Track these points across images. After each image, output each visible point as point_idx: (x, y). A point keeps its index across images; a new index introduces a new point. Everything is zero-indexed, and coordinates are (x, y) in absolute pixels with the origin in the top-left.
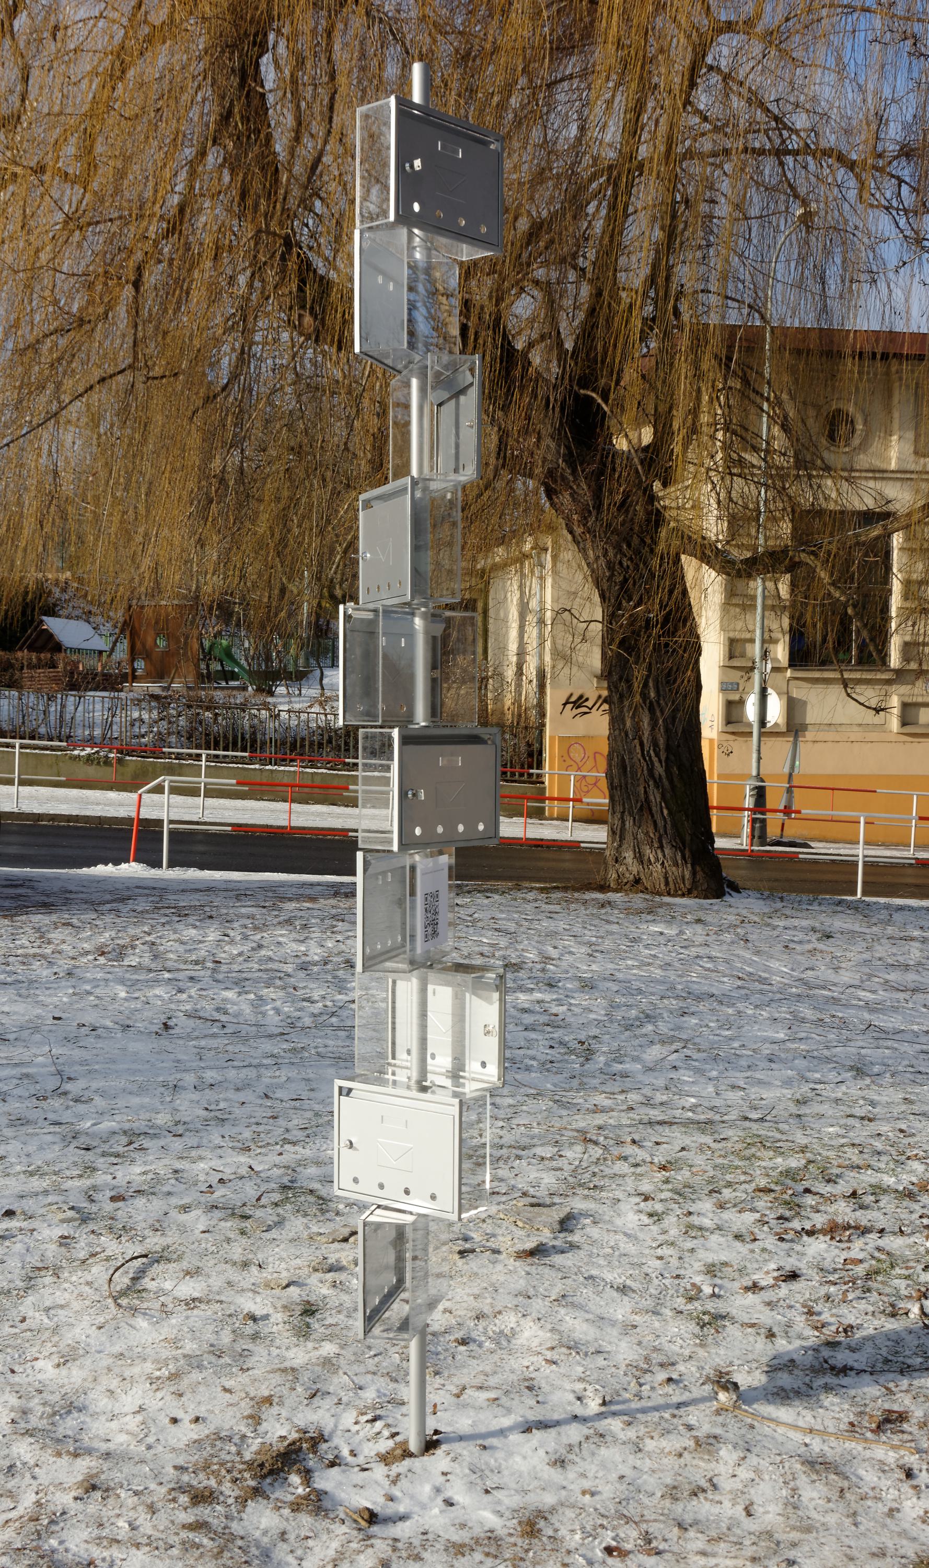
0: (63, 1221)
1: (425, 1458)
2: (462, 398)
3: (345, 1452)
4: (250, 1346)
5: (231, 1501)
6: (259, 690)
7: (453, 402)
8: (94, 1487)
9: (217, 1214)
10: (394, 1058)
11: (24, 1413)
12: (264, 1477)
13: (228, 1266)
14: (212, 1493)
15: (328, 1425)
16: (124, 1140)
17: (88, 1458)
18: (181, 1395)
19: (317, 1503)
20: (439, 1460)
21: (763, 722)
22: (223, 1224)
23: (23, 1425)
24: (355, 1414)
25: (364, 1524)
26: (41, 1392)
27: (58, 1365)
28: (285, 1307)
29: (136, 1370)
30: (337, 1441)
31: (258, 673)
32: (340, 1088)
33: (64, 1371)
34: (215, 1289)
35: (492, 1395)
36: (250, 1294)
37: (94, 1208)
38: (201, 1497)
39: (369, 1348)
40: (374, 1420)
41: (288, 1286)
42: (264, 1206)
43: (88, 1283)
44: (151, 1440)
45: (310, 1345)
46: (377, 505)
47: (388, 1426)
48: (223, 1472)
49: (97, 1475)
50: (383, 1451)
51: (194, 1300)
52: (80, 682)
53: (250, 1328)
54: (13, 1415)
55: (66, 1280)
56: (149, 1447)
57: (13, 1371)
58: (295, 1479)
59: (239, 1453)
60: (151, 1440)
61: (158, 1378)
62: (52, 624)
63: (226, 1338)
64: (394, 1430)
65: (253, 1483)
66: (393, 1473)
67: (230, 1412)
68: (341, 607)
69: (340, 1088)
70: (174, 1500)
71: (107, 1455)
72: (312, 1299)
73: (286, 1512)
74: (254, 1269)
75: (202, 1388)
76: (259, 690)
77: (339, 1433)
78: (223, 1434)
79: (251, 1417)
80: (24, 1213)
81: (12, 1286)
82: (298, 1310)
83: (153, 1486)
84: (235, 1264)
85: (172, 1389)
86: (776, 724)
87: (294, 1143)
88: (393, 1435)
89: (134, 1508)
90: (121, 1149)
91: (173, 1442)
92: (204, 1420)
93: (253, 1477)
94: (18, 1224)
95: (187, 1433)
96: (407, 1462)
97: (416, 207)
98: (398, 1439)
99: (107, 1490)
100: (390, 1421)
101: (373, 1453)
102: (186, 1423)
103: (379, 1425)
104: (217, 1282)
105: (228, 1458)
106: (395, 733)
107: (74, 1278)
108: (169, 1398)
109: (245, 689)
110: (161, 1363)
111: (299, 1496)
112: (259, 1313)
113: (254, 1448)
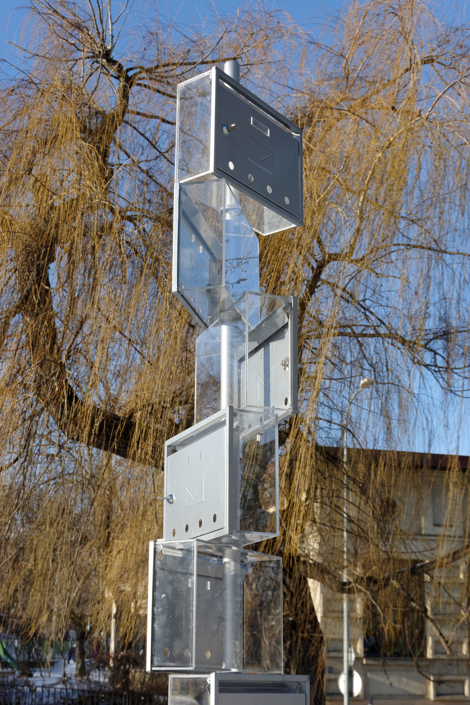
2: (273, 345)
6: (23, 674)
7: (262, 350)
21: (350, 693)
31: (23, 662)
46: (181, 452)
68: (151, 544)
76: (23, 674)
86: (358, 696)
97: (231, 166)
106: (211, 679)
109: (13, 673)
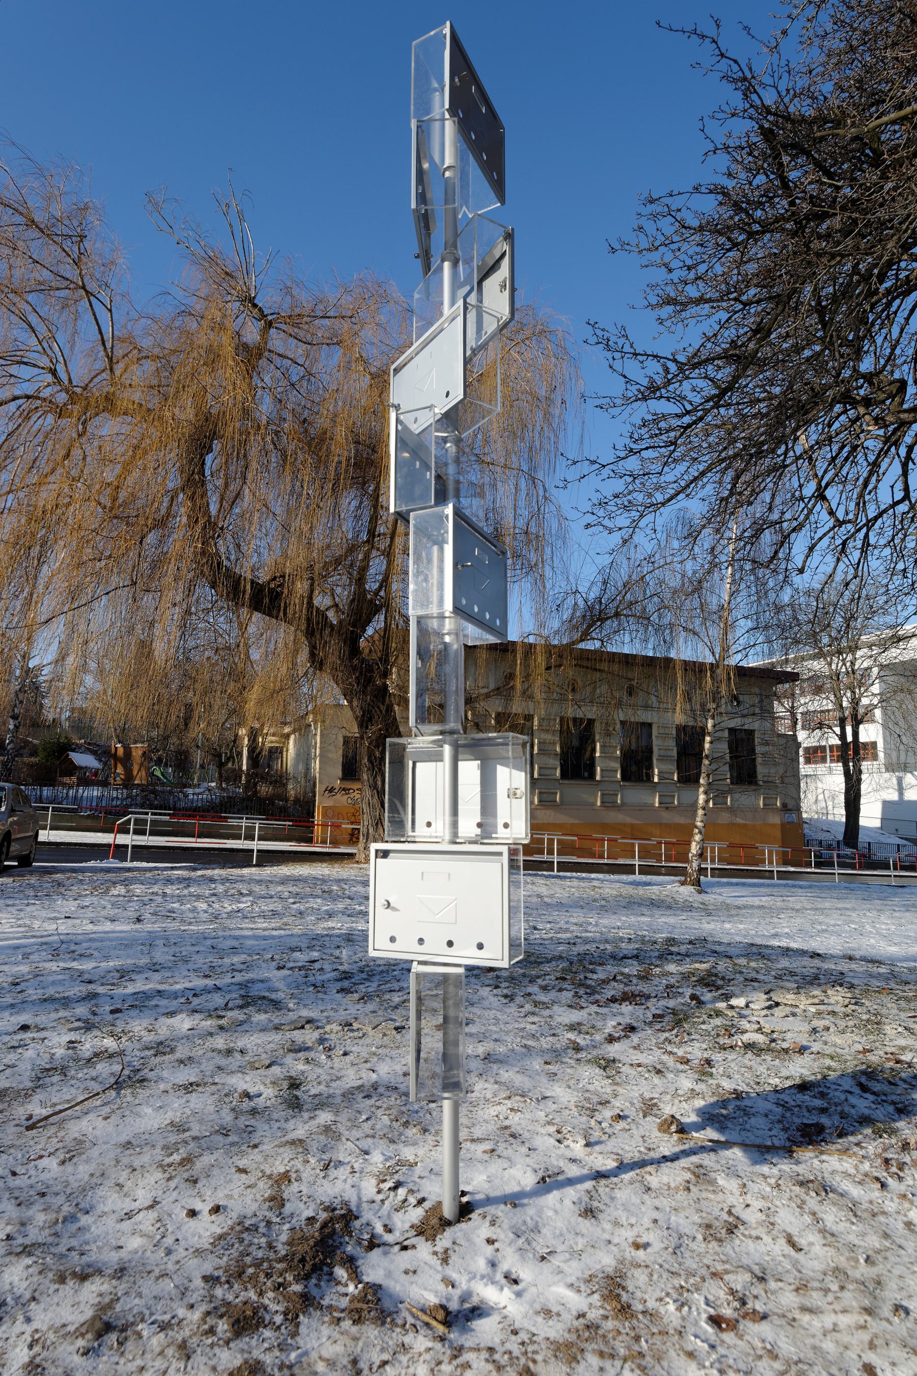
0: (71, 1030)
1: (463, 1226)
3: (379, 1229)
4: (252, 1122)
5: (278, 1319)
8: (108, 1327)
9: (198, 1016)
10: (413, 831)
11: (23, 1224)
12: (307, 1277)
13: (215, 1054)
14: (255, 1311)
15: (351, 1196)
16: (117, 975)
17: (97, 1280)
18: (196, 1182)
19: (376, 1306)
20: (477, 1228)
22: (203, 1023)
23: (20, 1240)
24: (374, 1182)
25: (441, 1329)
26: (43, 1195)
27: (63, 1162)
28: (273, 1083)
29: (146, 1158)
30: (367, 1215)
32: (377, 851)
33: (69, 1168)
34: (208, 1073)
35: (488, 1146)
36: (240, 1075)
37: (97, 1019)
38: (246, 1322)
39: (359, 1112)
40: (395, 1188)
41: (269, 1066)
42: (231, 1009)
43: (93, 1079)
44: (169, 1241)
45: (306, 1115)
47: (411, 1191)
48: (262, 1278)
49: (110, 1306)
50: (416, 1221)
51: (191, 1084)
52: (85, 782)
53: (246, 1105)
54: (9, 1229)
55: (72, 1078)
56: (169, 1252)
57: (14, 1174)
58: (341, 1273)
59: (270, 1246)
60: (169, 1241)
61: (170, 1165)
62: (73, 756)
63: (227, 1117)
64: (419, 1196)
65: (297, 1288)
66: (439, 1249)
67: (249, 1195)
69: (377, 851)
70: (212, 1331)
71: (121, 1272)
72: (293, 1074)
73: (347, 1324)
74: (237, 1055)
75: (216, 1171)
77: (365, 1205)
78: (248, 1223)
79: (272, 1199)
80: (36, 1026)
81: (21, 1086)
82: (285, 1085)
83: (181, 1312)
84: (220, 1052)
85: (186, 1175)
87: (241, 971)
88: (421, 1201)
89: (161, 1353)
90: (115, 981)
91: (195, 1242)
92: (225, 1208)
93: (297, 1279)
94: (31, 1035)
95: (206, 1228)
96: (449, 1232)
98: (427, 1205)
99: (123, 1330)
100: (411, 1186)
101: (407, 1226)
102: (205, 1216)
103: (402, 1192)
104: (208, 1067)
105: (260, 1254)
107: (80, 1075)
108: (183, 1186)
110: (169, 1149)
111: (354, 1299)
112: (252, 1091)
113: (284, 1237)
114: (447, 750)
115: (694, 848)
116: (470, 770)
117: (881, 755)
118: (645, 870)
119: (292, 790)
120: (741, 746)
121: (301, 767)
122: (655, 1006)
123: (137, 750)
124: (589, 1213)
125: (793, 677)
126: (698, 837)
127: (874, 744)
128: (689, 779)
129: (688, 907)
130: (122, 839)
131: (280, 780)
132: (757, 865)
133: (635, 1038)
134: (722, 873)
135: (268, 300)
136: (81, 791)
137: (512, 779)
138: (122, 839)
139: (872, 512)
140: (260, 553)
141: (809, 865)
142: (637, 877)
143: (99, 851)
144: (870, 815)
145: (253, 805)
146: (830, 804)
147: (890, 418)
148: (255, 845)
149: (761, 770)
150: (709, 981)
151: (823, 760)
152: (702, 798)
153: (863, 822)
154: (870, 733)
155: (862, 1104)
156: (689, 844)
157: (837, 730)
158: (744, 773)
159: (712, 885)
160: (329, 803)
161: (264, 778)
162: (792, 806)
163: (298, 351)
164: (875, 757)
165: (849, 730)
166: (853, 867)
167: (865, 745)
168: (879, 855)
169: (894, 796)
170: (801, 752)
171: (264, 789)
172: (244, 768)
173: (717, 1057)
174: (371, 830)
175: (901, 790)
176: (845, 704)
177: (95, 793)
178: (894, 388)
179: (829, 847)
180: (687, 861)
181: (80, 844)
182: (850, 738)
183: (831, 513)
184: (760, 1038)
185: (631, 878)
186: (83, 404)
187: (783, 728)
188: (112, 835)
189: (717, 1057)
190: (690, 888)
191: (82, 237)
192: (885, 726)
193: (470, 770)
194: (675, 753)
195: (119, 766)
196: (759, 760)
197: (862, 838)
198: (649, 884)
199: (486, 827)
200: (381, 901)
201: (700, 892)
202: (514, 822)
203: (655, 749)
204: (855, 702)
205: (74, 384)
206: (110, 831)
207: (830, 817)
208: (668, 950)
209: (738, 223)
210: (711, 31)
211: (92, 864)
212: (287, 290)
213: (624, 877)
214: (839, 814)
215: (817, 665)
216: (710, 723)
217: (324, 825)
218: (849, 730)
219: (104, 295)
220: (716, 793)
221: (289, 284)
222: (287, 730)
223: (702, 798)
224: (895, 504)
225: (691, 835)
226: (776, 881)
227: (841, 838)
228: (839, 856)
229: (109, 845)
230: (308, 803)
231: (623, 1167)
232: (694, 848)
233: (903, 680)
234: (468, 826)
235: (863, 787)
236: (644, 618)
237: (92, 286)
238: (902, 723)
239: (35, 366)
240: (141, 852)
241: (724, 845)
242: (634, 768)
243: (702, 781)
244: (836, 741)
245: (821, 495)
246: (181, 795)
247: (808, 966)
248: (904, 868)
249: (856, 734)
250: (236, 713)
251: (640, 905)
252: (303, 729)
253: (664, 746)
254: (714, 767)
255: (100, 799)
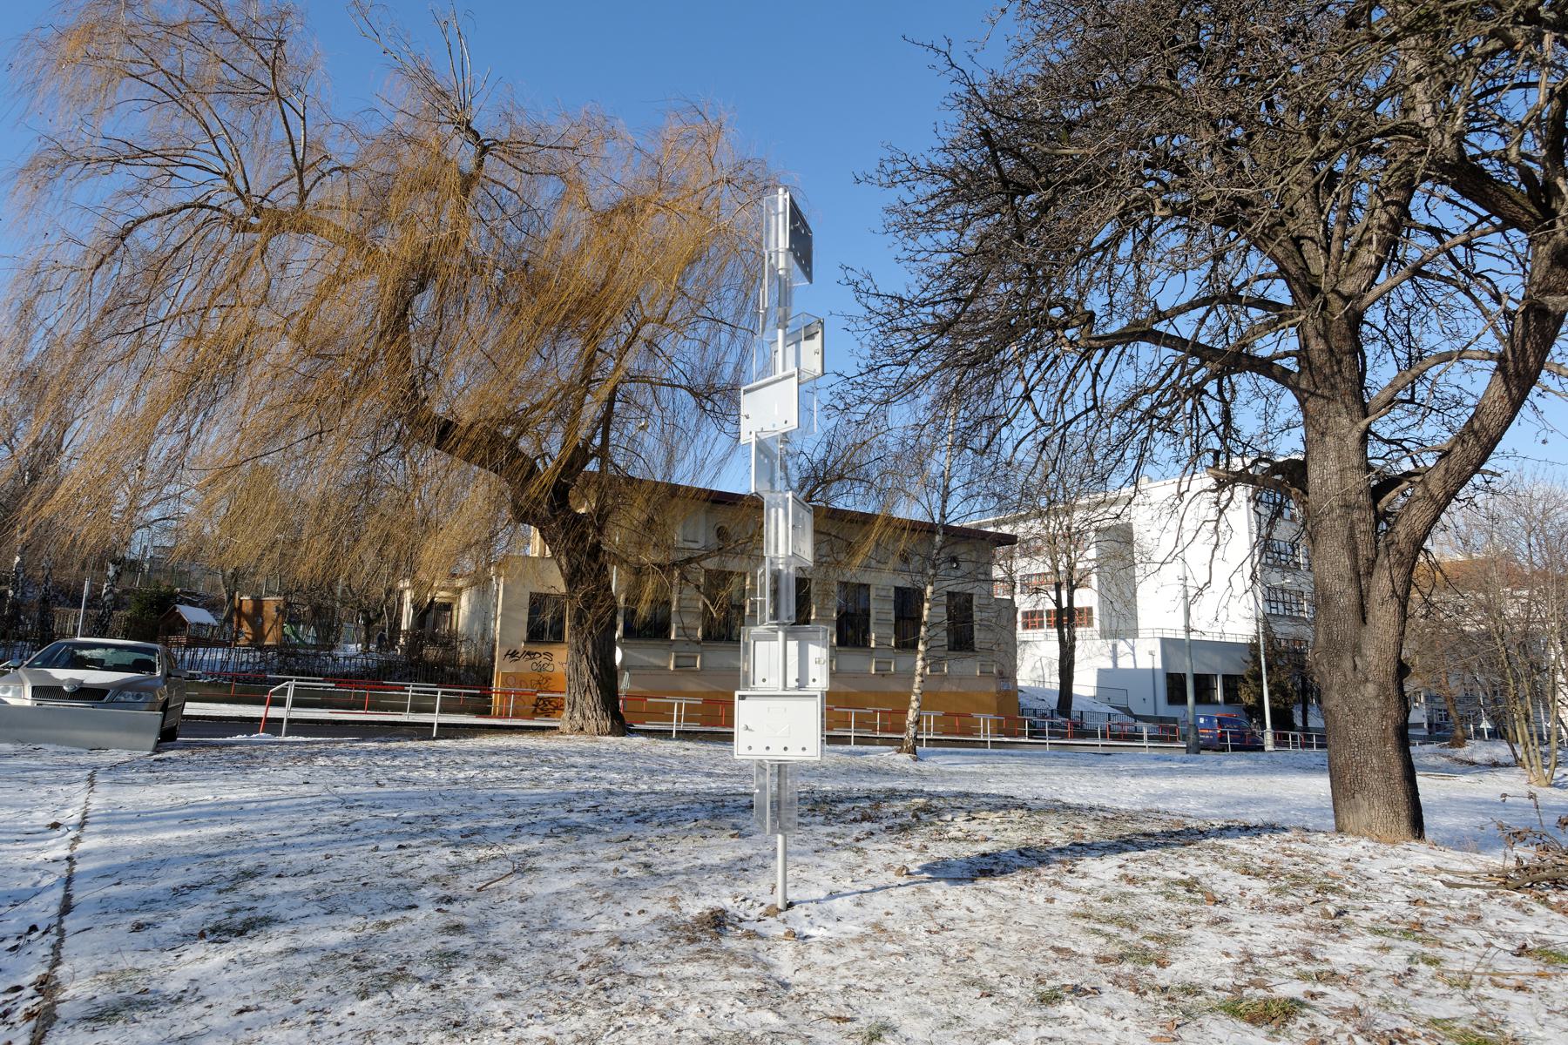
52: (196, 642)
114: (781, 634)
115: (911, 716)
116: (793, 646)
117: (1096, 623)
118: (860, 741)
119: (464, 653)
120: (960, 612)
121: (477, 627)
122: (886, 823)
123: (271, 604)
124: (858, 905)
125: (1010, 540)
126: (915, 705)
127: (1090, 610)
128: (907, 644)
129: (905, 774)
130: (275, 712)
131: (449, 642)
132: (971, 735)
133: (875, 838)
134: (938, 743)
135: (486, 124)
136: (200, 653)
137: (818, 653)
138: (275, 712)
139: (1069, 416)
140: (461, 392)
141: (1022, 734)
142: (853, 747)
143: (250, 724)
144: (1085, 685)
145: (418, 669)
146: (1047, 671)
147: (1081, 343)
148: (436, 718)
149: (978, 635)
150: (926, 809)
151: (1041, 626)
152: (920, 664)
153: (1076, 690)
154: (1085, 598)
155: (1018, 861)
156: (906, 712)
157: (1053, 595)
158: (961, 640)
159: (928, 754)
160: (511, 668)
161: (434, 639)
162: (1007, 674)
163: (514, 180)
164: (1090, 623)
165: (1064, 594)
166: (1064, 736)
167: (1081, 611)
168: (1089, 723)
169: (1109, 665)
170: (1019, 617)
171: (431, 653)
172: (404, 627)
173: (930, 845)
174: (578, 699)
175: (1115, 658)
176: (1061, 568)
177: (219, 656)
178: (1085, 317)
179: (1044, 716)
180: (903, 730)
181: (204, 717)
182: (1065, 604)
183: (1036, 413)
184: (960, 834)
185: (847, 748)
186: (264, 220)
187: (1000, 593)
188: (263, 708)
189: (930, 845)
190: (907, 756)
191: (281, 42)
192: (1100, 594)
193: (793, 646)
194: (892, 617)
195: (245, 623)
196: (976, 627)
197: (1076, 707)
198: (862, 753)
199: (802, 683)
200: (742, 726)
201: (915, 760)
202: (819, 679)
203: (873, 612)
204: (1071, 567)
205: (253, 192)
206: (261, 702)
207: (1047, 686)
208: (892, 794)
209: (964, 187)
210: (945, 48)
211: (239, 737)
212: (508, 117)
213: (840, 748)
214: (1054, 683)
215: (1036, 526)
216: (929, 589)
217: (505, 694)
218: (1064, 594)
219: (295, 100)
220: (934, 661)
221: (509, 110)
222: (459, 583)
223: (920, 664)
224: (1087, 411)
225: (909, 702)
226: (989, 750)
227: (1055, 706)
228: (1052, 725)
229: (260, 719)
230: (484, 668)
231: (875, 889)
232: (911, 716)
233: (1116, 545)
234: (792, 683)
235: (1077, 654)
236: (865, 480)
237: (284, 91)
238: (1114, 589)
239: (207, 169)
240: (297, 726)
241: (940, 714)
242: (850, 632)
243: (921, 647)
244: (1052, 607)
245: (1027, 397)
246: (330, 659)
247: (1002, 802)
248: (1113, 737)
249: (1070, 600)
250: (407, 563)
251: (858, 772)
252: (481, 583)
253: (881, 611)
254: (932, 633)
255: (224, 663)
